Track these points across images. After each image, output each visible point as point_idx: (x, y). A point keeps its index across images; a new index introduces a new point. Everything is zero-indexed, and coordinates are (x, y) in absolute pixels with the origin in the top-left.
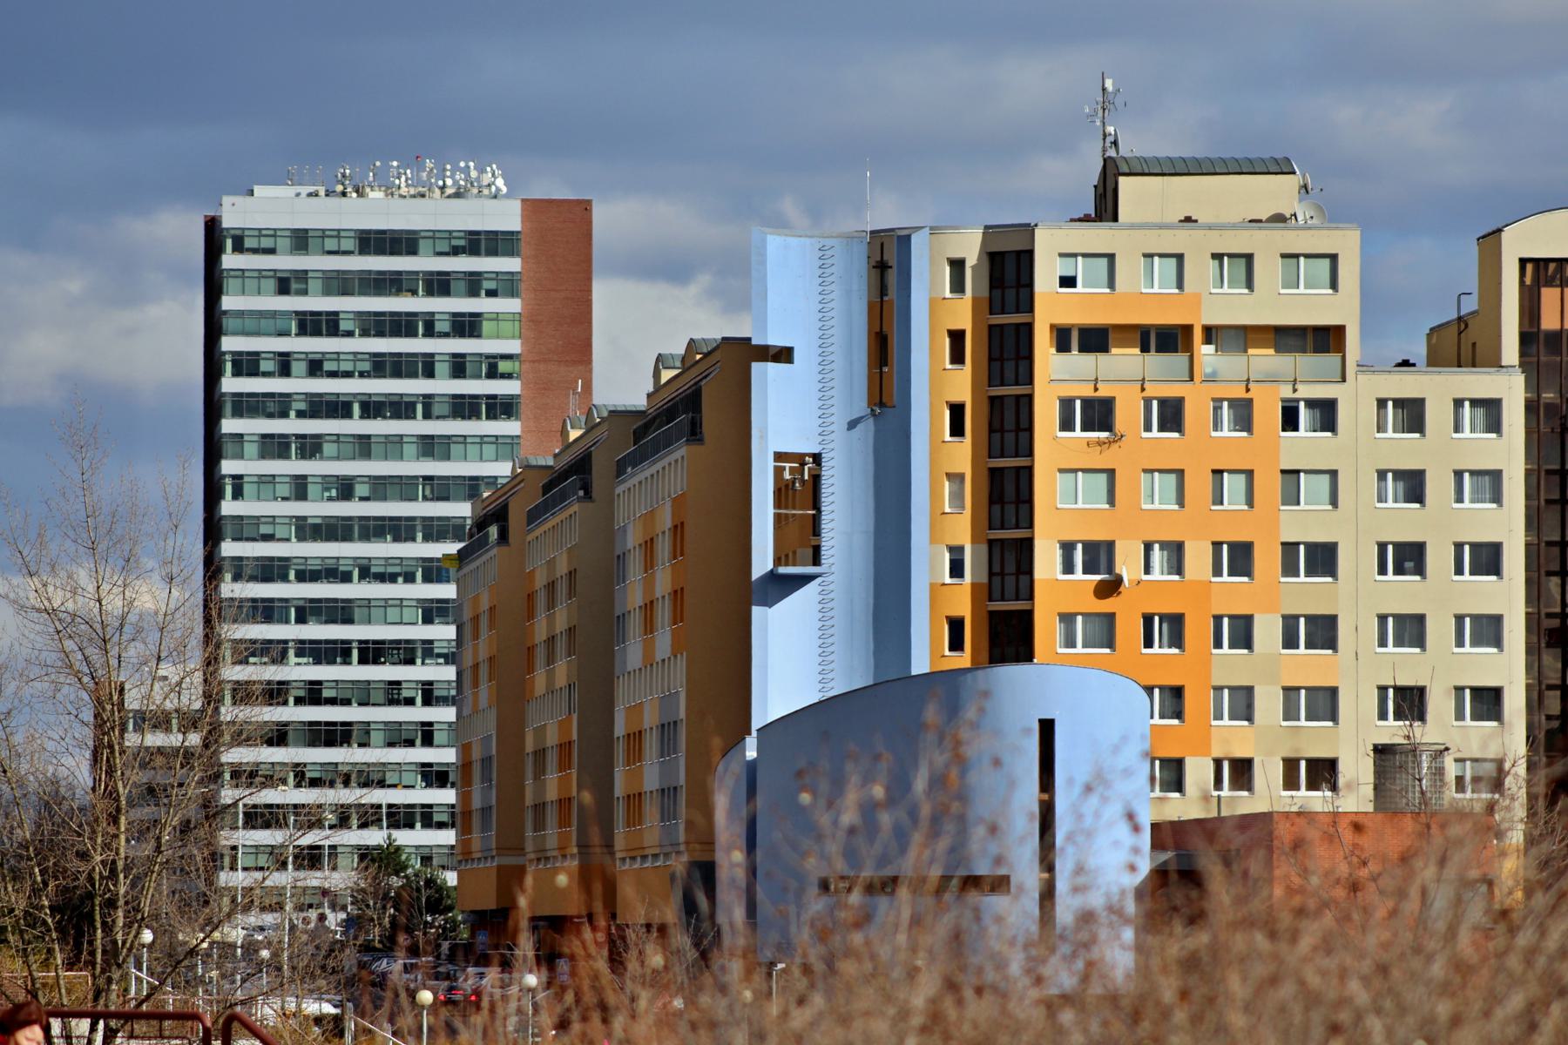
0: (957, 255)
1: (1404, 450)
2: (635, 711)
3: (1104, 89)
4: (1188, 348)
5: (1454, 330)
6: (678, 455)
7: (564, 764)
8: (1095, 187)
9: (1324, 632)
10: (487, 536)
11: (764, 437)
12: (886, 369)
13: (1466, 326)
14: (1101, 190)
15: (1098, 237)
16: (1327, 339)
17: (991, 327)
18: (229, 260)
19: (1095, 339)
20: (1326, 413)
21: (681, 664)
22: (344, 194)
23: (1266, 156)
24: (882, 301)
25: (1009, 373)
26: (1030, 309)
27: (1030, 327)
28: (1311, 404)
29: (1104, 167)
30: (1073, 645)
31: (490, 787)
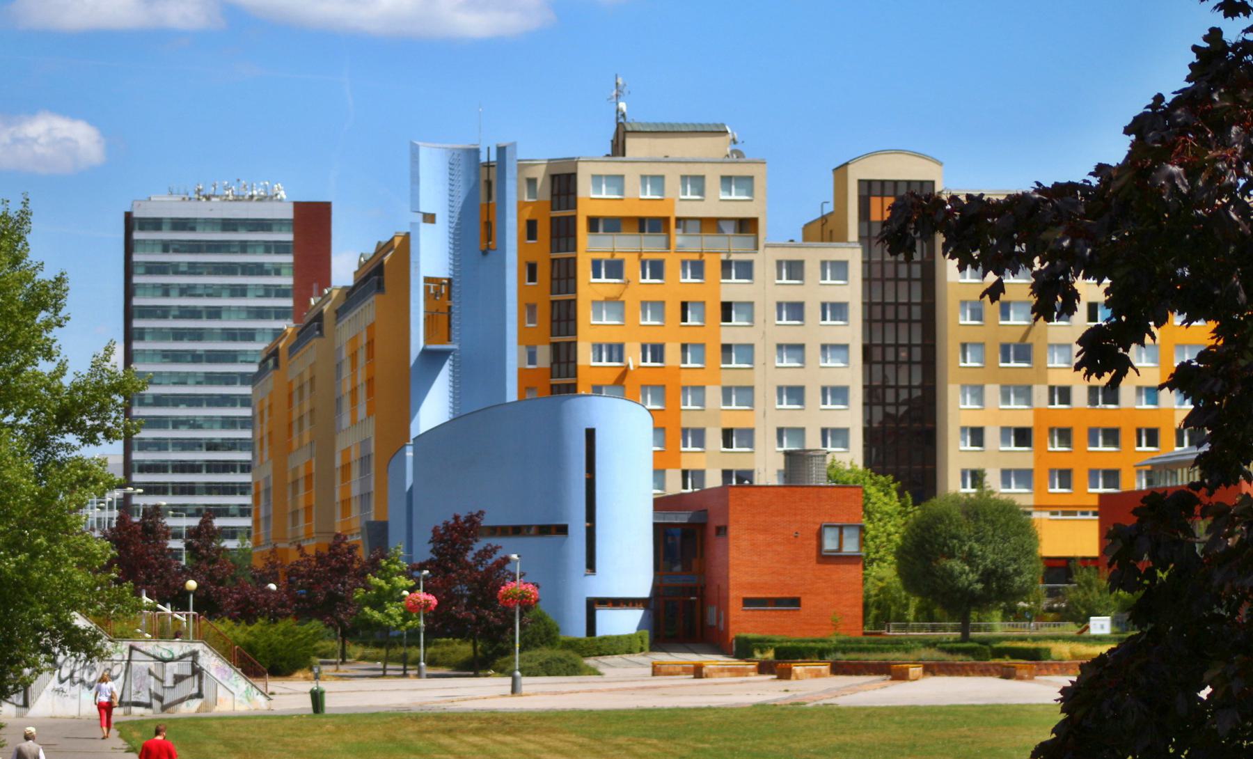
0: (532, 176)
1: (791, 291)
2: (346, 452)
3: (617, 84)
4: (667, 230)
5: (819, 224)
6: (369, 301)
7: (308, 487)
8: (612, 141)
9: (746, 393)
10: (268, 365)
11: (418, 268)
12: (490, 243)
13: (826, 221)
14: (615, 142)
15: (614, 168)
16: (747, 226)
17: (552, 219)
18: (137, 235)
19: (614, 225)
20: (746, 270)
21: (372, 421)
22: (199, 199)
23: (711, 122)
24: (488, 204)
25: (563, 246)
26: (575, 207)
27: (574, 218)
28: (739, 263)
29: (618, 129)
30: (600, 360)
31: (269, 504)
